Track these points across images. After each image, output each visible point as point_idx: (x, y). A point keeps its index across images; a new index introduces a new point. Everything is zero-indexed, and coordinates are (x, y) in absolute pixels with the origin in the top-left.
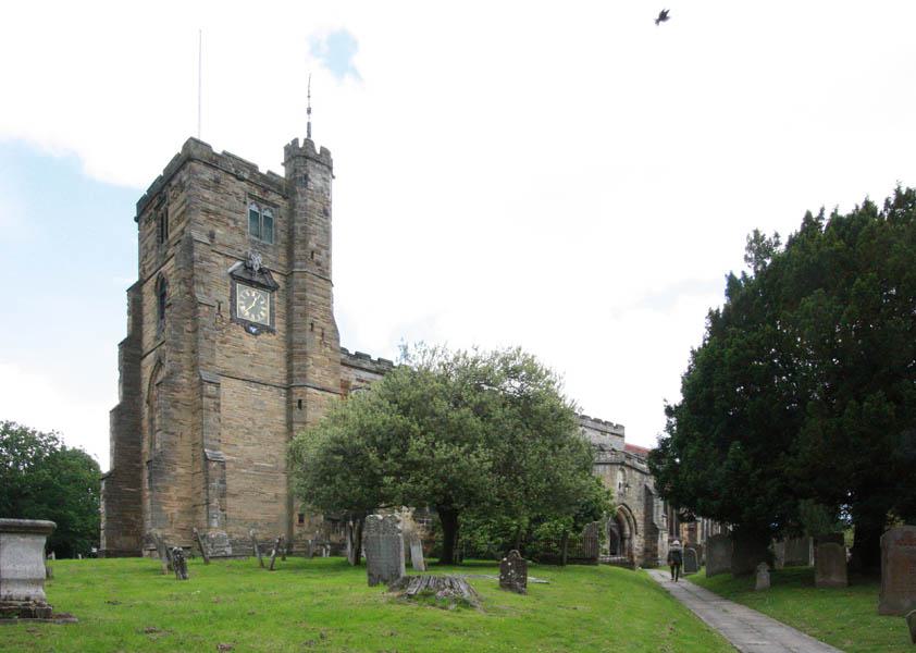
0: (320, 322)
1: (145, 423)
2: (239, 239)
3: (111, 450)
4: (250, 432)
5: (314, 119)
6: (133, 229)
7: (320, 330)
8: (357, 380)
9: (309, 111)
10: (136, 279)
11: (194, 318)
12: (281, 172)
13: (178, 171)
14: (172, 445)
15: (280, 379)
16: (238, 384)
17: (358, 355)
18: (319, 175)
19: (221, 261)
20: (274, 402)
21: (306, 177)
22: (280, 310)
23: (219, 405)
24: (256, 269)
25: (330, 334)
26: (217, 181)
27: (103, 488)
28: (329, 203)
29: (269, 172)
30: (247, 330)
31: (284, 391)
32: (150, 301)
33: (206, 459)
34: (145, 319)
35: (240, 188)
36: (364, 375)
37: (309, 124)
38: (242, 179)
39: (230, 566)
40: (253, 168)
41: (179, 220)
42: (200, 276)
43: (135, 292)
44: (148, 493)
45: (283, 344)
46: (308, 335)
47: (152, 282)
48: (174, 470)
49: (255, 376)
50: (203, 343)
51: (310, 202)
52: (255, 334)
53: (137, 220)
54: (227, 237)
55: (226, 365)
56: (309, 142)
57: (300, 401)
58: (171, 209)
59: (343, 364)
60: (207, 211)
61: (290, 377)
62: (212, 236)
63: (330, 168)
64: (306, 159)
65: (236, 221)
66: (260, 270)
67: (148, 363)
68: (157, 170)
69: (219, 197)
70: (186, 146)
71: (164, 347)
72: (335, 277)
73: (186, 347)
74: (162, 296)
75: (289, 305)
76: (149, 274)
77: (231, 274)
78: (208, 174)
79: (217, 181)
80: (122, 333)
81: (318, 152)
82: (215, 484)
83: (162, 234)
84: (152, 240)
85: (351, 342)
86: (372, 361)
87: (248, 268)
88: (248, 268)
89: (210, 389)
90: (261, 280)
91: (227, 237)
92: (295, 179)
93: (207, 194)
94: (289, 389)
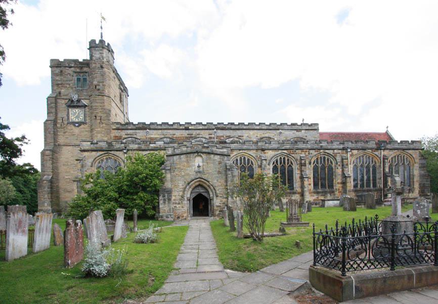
8: (126, 134)
29: (84, 60)
35: (70, 71)
36: (129, 132)
37: (101, 33)
56: (102, 41)
79: (61, 71)
81: (106, 44)
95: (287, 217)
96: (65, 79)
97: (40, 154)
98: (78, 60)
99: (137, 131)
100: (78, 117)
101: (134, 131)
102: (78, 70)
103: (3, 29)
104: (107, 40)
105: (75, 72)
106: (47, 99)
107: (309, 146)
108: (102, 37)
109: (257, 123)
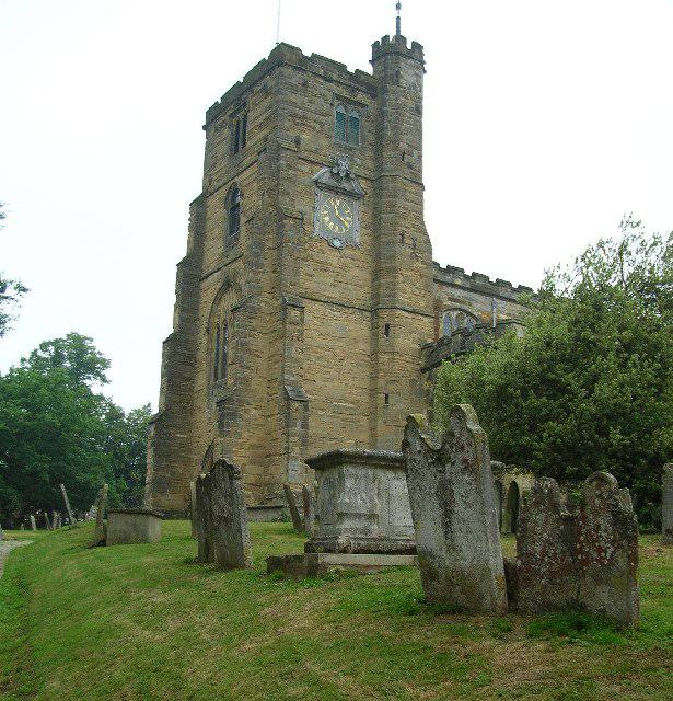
0: (411, 232)
2: (324, 142)
3: (162, 388)
4: (334, 366)
5: (402, 14)
6: (200, 139)
7: (411, 242)
8: (450, 299)
9: (398, 6)
10: (200, 191)
11: (279, 233)
12: (369, 69)
14: (247, 381)
15: (361, 295)
17: (451, 270)
19: (306, 168)
20: (359, 327)
25: (422, 245)
26: (305, 84)
27: (152, 434)
28: (421, 99)
31: (368, 314)
32: (217, 212)
33: (288, 398)
35: (320, 86)
36: (457, 293)
37: (398, 18)
38: (331, 81)
40: (341, 67)
42: (285, 186)
43: (199, 207)
45: (369, 259)
47: (222, 193)
48: (247, 411)
50: (288, 260)
53: (205, 128)
54: (310, 145)
56: (400, 39)
57: (387, 327)
58: (251, 115)
59: (436, 281)
60: (294, 116)
61: (375, 296)
62: (298, 141)
63: (423, 63)
64: (397, 56)
67: (210, 287)
71: (240, 264)
72: (427, 177)
73: (267, 264)
74: (234, 209)
75: (376, 214)
76: (216, 184)
78: (297, 78)
79: (305, 84)
81: (409, 46)
82: (298, 429)
84: (224, 148)
85: (443, 256)
86: (466, 277)
91: (310, 145)
92: (385, 78)
94: (374, 311)
95: (290, 532)
97: (175, 270)
99: (473, 295)
101: (466, 293)
104: (410, 34)
105: (338, 97)
106: (230, 120)
107: (337, 295)
109: (515, 286)
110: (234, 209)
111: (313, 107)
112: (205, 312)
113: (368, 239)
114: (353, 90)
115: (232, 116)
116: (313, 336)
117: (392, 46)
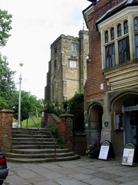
1: (51, 89)
6: (50, 50)
13: (59, 40)
16: (70, 81)
18: (85, 36)
19: (67, 56)
21: (83, 37)
22: (78, 64)
23: (66, 86)
24: (73, 57)
29: (76, 37)
30: (72, 69)
32: (53, 64)
33: (64, 97)
34: (52, 68)
35: (49, 119)
37: (84, 26)
39: (123, 168)
41: (59, 49)
43: (50, 63)
44: (87, 125)
46: (84, 69)
47: (53, 61)
49: (73, 78)
51: (84, 42)
52: (73, 70)
55: (68, 77)
57: (82, 83)
65: (69, 48)
66: (74, 57)
67: (52, 77)
68: (55, 39)
69: (66, 44)
70: (61, 36)
76: (53, 59)
77: (69, 59)
78: (64, 40)
79: (66, 41)
80: (47, 71)
83: (56, 52)
84: (53, 52)
87: (72, 57)
88: (72, 57)
89: (64, 82)
90: (75, 59)
93: (65, 44)
96: (68, 45)
97: (46, 74)
98: (73, 37)
100: (73, 65)
102: (73, 42)
103: (12, 16)
105: (72, 43)
108: (84, 28)
110: (55, 64)
111: (68, 45)
112: (51, 82)
113: (79, 68)
114: (75, 41)
115: (55, 46)
116: (77, 77)
117: (82, 32)
